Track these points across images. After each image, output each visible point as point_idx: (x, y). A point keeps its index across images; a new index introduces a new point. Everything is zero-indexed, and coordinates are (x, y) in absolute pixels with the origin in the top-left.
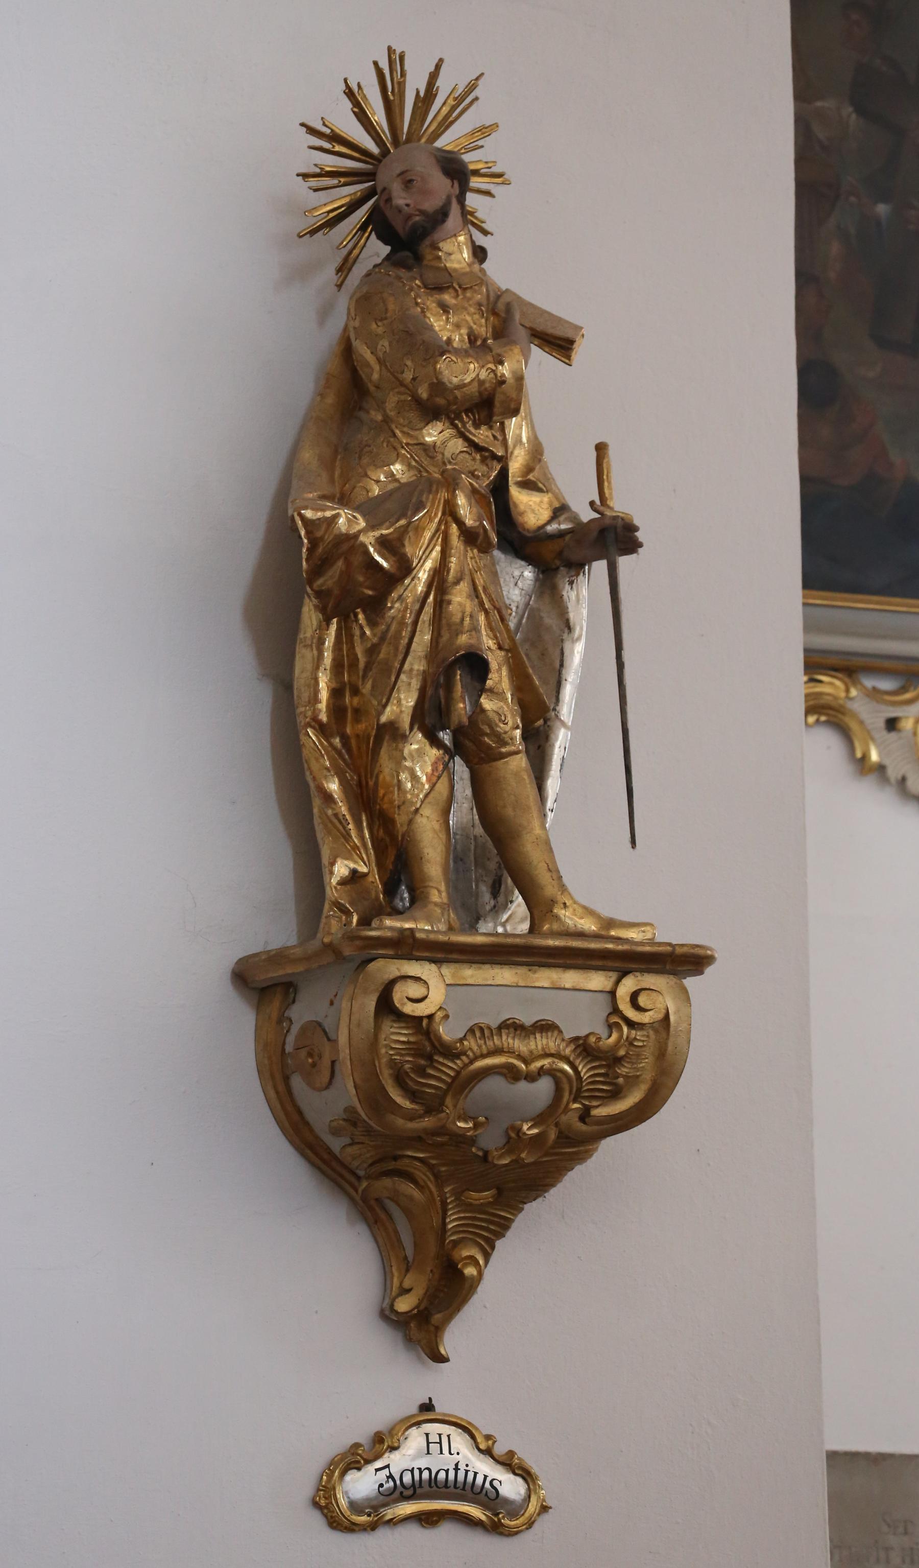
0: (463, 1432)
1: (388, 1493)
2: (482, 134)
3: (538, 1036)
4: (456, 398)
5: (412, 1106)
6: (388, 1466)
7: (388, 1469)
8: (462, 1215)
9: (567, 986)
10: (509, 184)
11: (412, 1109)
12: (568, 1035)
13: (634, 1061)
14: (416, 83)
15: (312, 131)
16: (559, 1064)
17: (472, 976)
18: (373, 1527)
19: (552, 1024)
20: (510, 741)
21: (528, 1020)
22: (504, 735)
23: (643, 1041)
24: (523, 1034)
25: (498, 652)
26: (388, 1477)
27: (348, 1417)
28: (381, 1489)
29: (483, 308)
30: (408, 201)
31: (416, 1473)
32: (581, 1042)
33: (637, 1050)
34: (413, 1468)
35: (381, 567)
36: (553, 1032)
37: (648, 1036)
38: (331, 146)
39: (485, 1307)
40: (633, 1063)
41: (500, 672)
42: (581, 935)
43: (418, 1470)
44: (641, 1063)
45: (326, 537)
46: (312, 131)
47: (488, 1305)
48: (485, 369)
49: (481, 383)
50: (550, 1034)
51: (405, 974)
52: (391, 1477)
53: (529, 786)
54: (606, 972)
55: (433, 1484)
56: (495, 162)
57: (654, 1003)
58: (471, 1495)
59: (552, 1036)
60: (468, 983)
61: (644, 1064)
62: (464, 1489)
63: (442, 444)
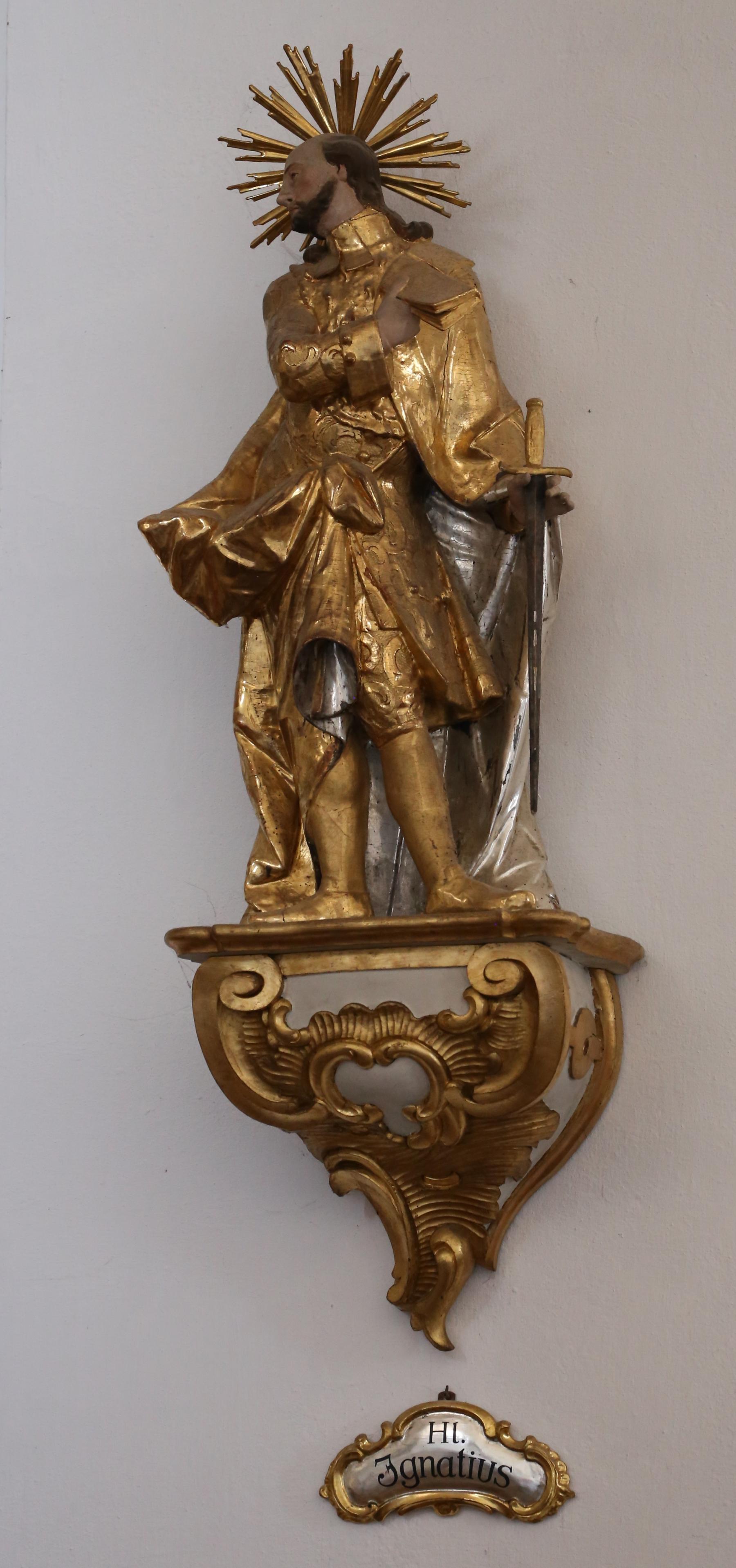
0: (472, 1420)
1: (389, 1484)
2: (420, 108)
3: (383, 1019)
4: (301, 386)
5: (282, 1100)
6: (388, 1457)
7: (388, 1460)
8: (433, 1202)
9: (413, 965)
10: (467, 152)
11: (282, 1102)
12: (418, 1015)
13: (510, 1034)
14: (330, 75)
15: (233, 144)
16: (406, 1046)
17: (311, 965)
18: (379, 1517)
19: (396, 1006)
20: (396, 721)
21: (371, 1003)
22: (387, 716)
23: (517, 1013)
24: (365, 1019)
25: (381, 632)
26: (388, 1468)
27: (362, 1409)
28: (381, 1480)
29: (368, 289)
30: (290, 196)
31: (418, 1463)
32: (434, 1020)
33: (511, 1022)
34: (414, 1458)
35: (243, 568)
36: (398, 1013)
37: (521, 1008)
38: (260, 154)
39: (513, 1291)
40: (510, 1037)
41: (381, 653)
42: (458, 910)
43: (419, 1460)
44: (518, 1036)
45: (171, 545)
46: (233, 144)
47: (516, 1289)
48: (328, 352)
49: (327, 368)
50: (395, 1016)
51: (240, 970)
52: (391, 1467)
53: (416, 764)
54: (460, 947)
55: (436, 1472)
56: (448, 133)
57: (504, 974)
58: (479, 1483)
59: (398, 1016)
60: (306, 972)
61: (522, 1037)
62: (470, 1476)
63: (320, 433)
